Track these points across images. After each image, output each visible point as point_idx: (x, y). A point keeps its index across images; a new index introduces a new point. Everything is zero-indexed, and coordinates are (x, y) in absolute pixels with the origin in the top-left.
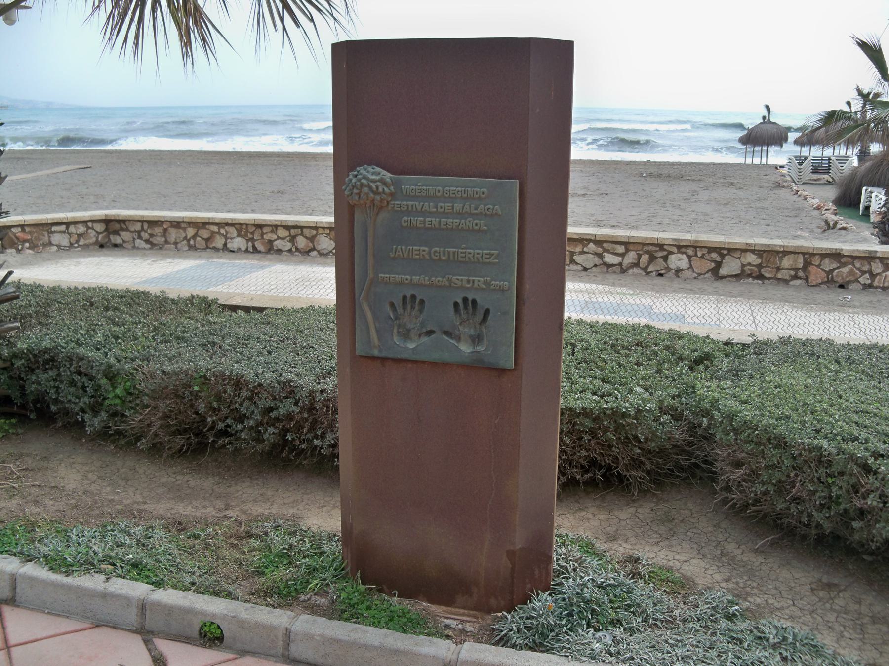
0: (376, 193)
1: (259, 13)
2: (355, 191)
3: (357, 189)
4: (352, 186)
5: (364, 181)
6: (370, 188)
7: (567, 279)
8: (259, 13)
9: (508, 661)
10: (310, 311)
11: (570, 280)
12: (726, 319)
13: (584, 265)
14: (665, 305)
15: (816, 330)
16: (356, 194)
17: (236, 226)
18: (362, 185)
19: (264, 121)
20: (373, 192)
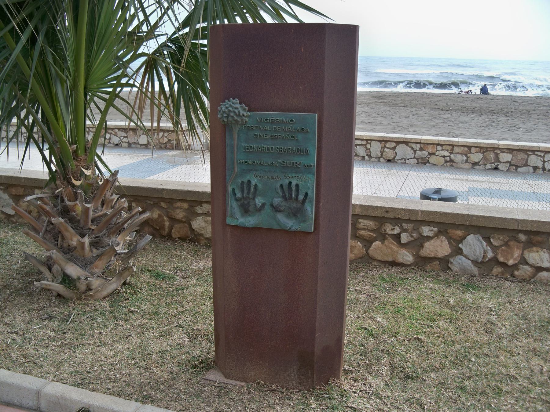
0: (239, 115)
1: (99, 48)
2: (225, 115)
3: (226, 114)
4: (223, 111)
5: (230, 109)
6: (235, 112)
7: (1, 145)
8: (99, 48)
9: (115, 407)
10: (39, 171)
11: (11, 147)
12: (472, 193)
13: (435, 156)
14: (458, 185)
15: (534, 206)
16: (225, 117)
17: (414, 146)
18: (230, 111)
19: (458, 65)
20: (236, 115)
